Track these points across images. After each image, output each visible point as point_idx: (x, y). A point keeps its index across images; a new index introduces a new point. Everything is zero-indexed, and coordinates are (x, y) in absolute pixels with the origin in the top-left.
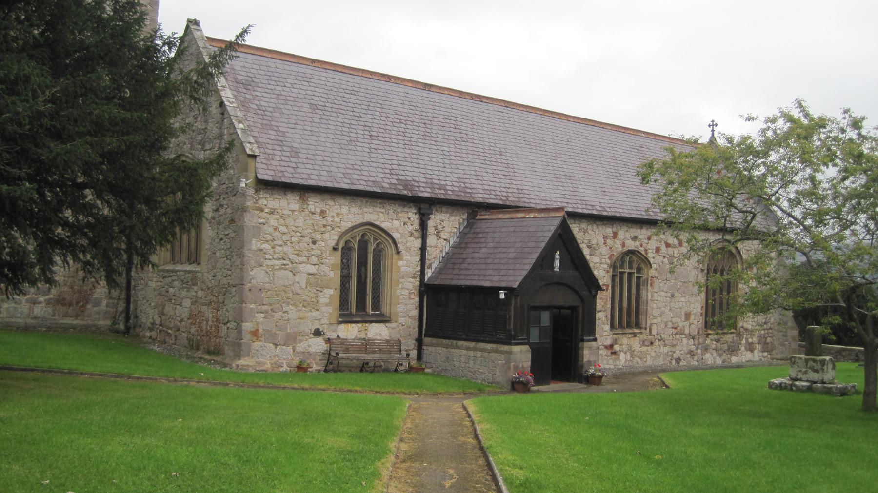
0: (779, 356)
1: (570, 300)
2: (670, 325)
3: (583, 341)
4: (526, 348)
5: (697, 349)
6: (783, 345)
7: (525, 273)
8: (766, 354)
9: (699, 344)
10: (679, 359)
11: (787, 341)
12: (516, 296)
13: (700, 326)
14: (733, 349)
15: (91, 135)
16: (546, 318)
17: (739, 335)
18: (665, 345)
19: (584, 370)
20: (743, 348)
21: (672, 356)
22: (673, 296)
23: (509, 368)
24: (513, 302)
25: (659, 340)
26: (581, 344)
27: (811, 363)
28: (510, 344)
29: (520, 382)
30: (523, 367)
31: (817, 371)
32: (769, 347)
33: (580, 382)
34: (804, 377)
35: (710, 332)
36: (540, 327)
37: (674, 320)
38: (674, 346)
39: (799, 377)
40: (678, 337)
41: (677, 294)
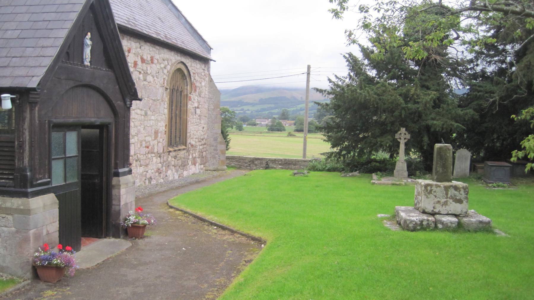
0: (211, 168)
1: (103, 116)
2: (144, 144)
3: (117, 175)
4: (51, 198)
5: (162, 167)
7: (48, 62)
8: (202, 166)
9: (164, 161)
10: (151, 178)
11: (217, 154)
12: (33, 104)
13: (165, 144)
14: (184, 166)
15: (240, 285)
16: (72, 142)
17: (188, 151)
18: (141, 166)
19: (122, 217)
20: (190, 163)
21: (146, 175)
22: (146, 114)
23: (26, 240)
24: (28, 115)
25: (136, 161)
26: (114, 180)
27: (452, 192)
28: (26, 195)
29: (51, 267)
30: (48, 233)
31: (460, 201)
33: (116, 236)
34: (443, 210)
35: (171, 149)
36: (65, 159)
37: (147, 138)
38: (147, 165)
39: (436, 210)
40: (149, 156)
41: (149, 113)
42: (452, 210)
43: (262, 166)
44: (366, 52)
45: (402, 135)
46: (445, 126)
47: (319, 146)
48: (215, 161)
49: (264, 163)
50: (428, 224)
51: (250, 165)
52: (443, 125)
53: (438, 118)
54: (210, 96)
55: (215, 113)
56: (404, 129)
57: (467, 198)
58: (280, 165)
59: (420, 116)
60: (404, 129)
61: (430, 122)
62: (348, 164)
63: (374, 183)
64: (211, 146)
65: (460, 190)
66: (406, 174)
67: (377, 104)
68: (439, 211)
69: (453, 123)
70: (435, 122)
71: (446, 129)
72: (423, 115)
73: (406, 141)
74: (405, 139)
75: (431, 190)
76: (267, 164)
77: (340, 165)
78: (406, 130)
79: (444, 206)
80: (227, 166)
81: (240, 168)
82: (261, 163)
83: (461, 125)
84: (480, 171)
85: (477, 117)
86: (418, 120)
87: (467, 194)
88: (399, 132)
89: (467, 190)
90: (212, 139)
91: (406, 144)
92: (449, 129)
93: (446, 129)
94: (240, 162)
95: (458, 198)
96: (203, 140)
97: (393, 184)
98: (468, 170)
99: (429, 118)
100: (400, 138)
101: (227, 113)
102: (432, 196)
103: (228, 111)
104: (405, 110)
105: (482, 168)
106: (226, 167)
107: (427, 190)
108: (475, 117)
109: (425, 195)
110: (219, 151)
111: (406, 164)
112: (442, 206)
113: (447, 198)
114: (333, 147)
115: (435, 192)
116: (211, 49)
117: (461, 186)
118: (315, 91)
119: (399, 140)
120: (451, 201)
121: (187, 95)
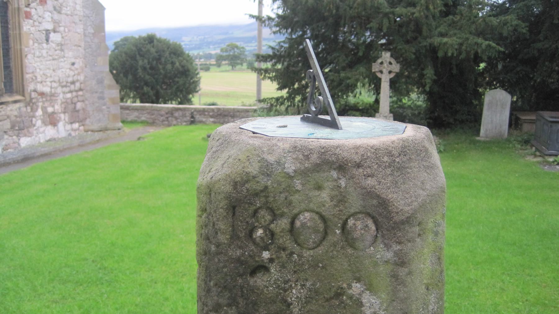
0: (95, 127)
6: (100, 110)
11: (105, 104)
20: (39, 123)
43: (185, 119)
45: (385, 65)
46: (464, 47)
47: (271, 89)
49: (187, 114)
51: (167, 118)
52: (461, 44)
53: (451, 33)
54: (87, 12)
56: (388, 54)
59: (418, 30)
60: (388, 54)
61: (437, 40)
67: (338, 8)
69: (480, 40)
70: (445, 40)
71: (468, 53)
72: (425, 28)
73: (392, 75)
74: (390, 72)
76: (192, 117)
78: (392, 56)
80: (123, 122)
81: (152, 123)
82: (184, 116)
83: (494, 45)
84: (526, 127)
85: (524, 31)
86: (415, 38)
88: (379, 61)
90: (94, 82)
91: (393, 83)
92: (472, 52)
93: (468, 53)
94: (153, 115)
96: (73, 83)
98: (506, 127)
99: (437, 33)
100: (381, 72)
101: (236, 50)
103: (237, 47)
104: (389, 18)
105: (532, 122)
106: (120, 124)
108: (520, 30)
114: (280, 89)
119: (379, 75)
121: (19, 9)
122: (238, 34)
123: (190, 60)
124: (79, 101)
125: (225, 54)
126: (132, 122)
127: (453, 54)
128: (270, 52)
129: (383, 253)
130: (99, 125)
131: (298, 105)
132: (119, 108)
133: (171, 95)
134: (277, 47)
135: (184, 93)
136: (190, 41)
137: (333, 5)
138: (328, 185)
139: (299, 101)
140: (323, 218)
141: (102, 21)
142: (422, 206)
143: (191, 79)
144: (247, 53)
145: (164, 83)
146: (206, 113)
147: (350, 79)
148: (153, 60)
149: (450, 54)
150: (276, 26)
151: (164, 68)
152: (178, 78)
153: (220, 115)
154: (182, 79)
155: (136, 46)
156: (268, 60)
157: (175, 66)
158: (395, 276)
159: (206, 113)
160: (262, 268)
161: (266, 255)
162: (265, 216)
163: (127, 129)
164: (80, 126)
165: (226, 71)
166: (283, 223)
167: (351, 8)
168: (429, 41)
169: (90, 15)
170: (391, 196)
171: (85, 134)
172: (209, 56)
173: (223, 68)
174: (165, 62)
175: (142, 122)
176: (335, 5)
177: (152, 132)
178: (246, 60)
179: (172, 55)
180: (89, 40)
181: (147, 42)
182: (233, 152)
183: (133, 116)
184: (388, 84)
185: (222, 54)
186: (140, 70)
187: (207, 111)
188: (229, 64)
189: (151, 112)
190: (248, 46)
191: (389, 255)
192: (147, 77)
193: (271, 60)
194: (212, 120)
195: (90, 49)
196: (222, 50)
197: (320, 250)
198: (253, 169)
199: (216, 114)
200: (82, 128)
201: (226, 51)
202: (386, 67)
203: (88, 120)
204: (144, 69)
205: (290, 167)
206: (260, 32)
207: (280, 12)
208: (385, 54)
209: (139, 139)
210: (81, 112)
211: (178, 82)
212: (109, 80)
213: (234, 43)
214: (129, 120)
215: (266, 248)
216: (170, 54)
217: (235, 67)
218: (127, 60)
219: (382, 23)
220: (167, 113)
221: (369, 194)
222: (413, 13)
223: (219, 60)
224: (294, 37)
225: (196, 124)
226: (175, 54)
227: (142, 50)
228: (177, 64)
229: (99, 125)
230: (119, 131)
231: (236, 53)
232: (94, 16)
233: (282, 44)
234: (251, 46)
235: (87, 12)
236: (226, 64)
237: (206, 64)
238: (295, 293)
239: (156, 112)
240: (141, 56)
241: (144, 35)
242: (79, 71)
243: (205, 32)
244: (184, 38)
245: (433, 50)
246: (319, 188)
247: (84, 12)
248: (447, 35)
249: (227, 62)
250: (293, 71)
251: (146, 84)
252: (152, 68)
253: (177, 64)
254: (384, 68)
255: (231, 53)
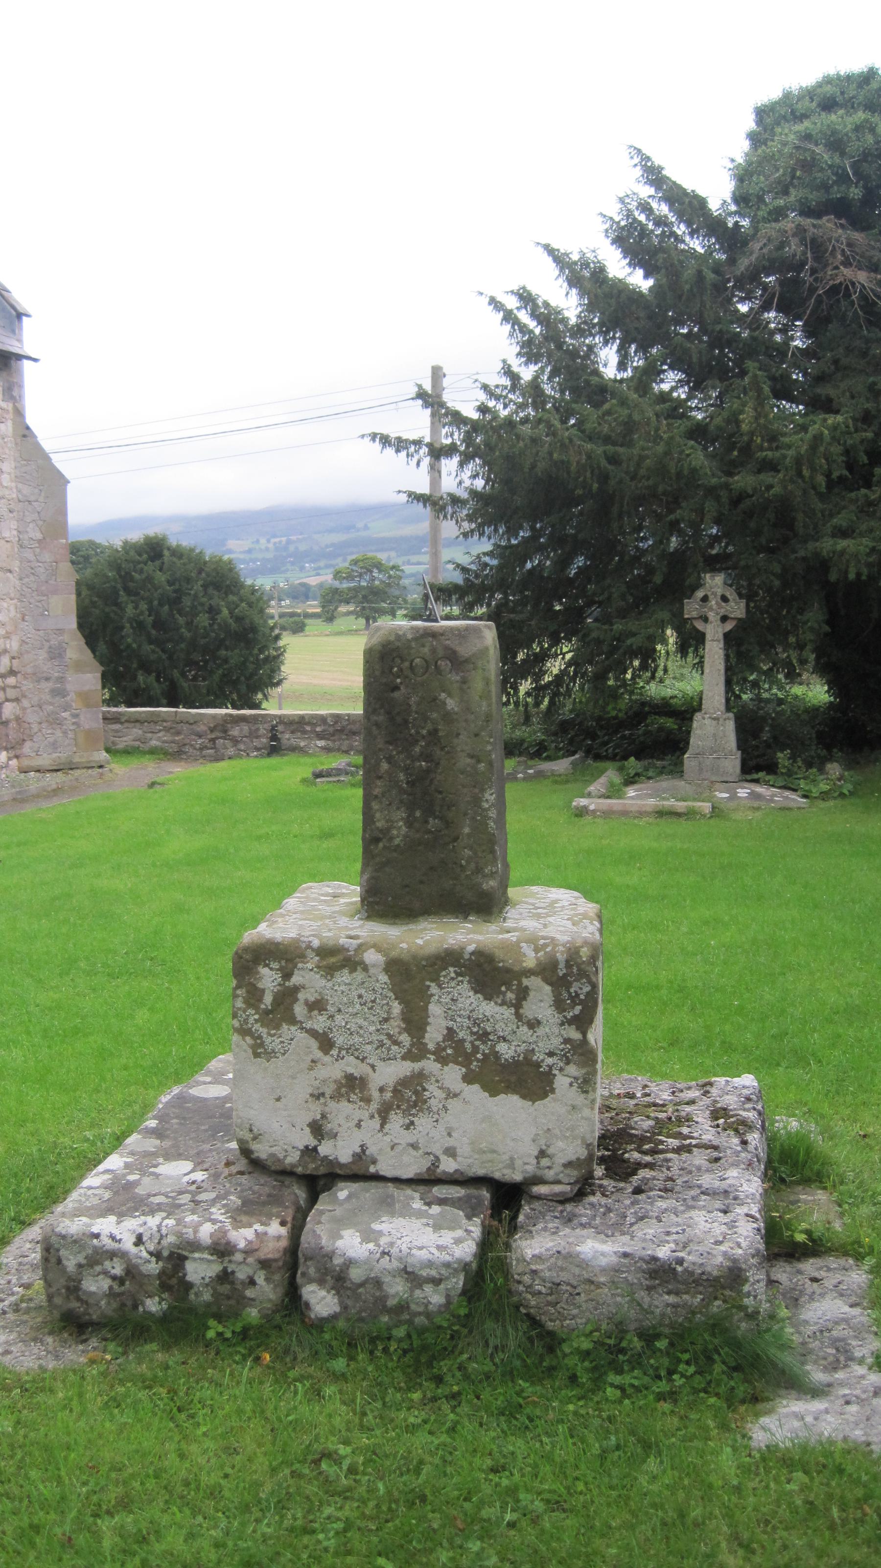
0: (45, 760)
6: (55, 721)
27: (454, 1005)
31: (526, 1079)
32: (13, 735)
34: (396, 1149)
39: (340, 1150)
42: (464, 1149)
43: (256, 743)
44: (585, 277)
48: (59, 733)
49: (262, 731)
50: (225, 1277)
51: (213, 740)
53: (864, 527)
55: (47, 557)
57: (582, 1053)
58: (320, 736)
61: (827, 545)
62: (564, 727)
63: (581, 812)
64: (39, 677)
65: (523, 994)
66: (733, 763)
68: (361, 1156)
70: (842, 544)
73: (729, 626)
74: (724, 619)
75: (287, 996)
76: (274, 738)
77: (534, 733)
79: (396, 1120)
80: (108, 750)
81: (177, 754)
82: (253, 735)
87: (583, 1022)
88: (700, 594)
89: (581, 988)
90: (43, 655)
94: (178, 733)
95: (506, 1051)
97: (661, 814)
100: (706, 620)
102: (294, 1040)
103: (379, 566)
104: (718, 499)
107: (254, 995)
109: (244, 1031)
110: (72, 696)
111: (730, 726)
112: (384, 1114)
113: (417, 1052)
115: (317, 1006)
116: (20, 316)
117: (530, 959)
118: (377, 445)
119: (699, 625)
120: (453, 1075)
122: (380, 529)
123: (256, 600)
124: (7, 700)
125: (345, 585)
126: (128, 752)
127: (859, 575)
128: (458, 578)
129: (455, 677)
130: (55, 755)
131: (526, 705)
132: (101, 716)
133: (208, 694)
134: (473, 567)
135: (243, 688)
136: (250, 551)
137: (592, 473)
138: (428, 644)
139: (528, 694)
140: (426, 661)
141: (62, 511)
142: (474, 655)
143: (261, 651)
144: (405, 582)
145: (191, 663)
146: (308, 728)
147: (634, 635)
148: (161, 605)
149: (852, 576)
150: (470, 518)
151: (189, 624)
152: (227, 649)
153: (341, 731)
154: (237, 651)
155: (119, 568)
156: (454, 598)
157: (219, 618)
158: (461, 689)
159: (308, 728)
160: (396, 688)
161: (399, 680)
162: (398, 661)
163: (119, 768)
164: (9, 759)
165: (350, 632)
166: (407, 664)
167: (632, 479)
168: (811, 546)
169: (32, 498)
170: (458, 649)
171: (22, 776)
172: (302, 593)
173: (341, 623)
174: (193, 607)
175: (152, 752)
176: (596, 472)
177: (178, 772)
178: (405, 601)
179: (211, 590)
180: (31, 556)
181: (145, 556)
182: (382, 632)
183: (130, 736)
184: (722, 645)
185: (337, 584)
186: (128, 630)
187: (309, 723)
188: (357, 614)
189: (174, 726)
190: (409, 563)
191: (458, 678)
192: (148, 648)
193: (461, 597)
194: (321, 743)
195: (32, 578)
196: (337, 575)
197: (425, 677)
198: (392, 638)
199: (331, 729)
200: (14, 763)
201: (350, 577)
202: (715, 607)
203: (28, 744)
204: (139, 626)
205: (410, 636)
206: (435, 530)
207: (479, 484)
208: (712, 578)
209: (152, 785)
210: (13, 725)
211: (226, 661)
212: (76, 649)
213: (370, 555)
214: (121, 746)
215: (399, 677)
216: (205, 587)
217: (375, 621)
218: (93, 604)
219: (703, 509)
220: (212, 730)
221: (447, 648)
222: (769, 487)
223: (330, 602)
224: (514, 542)
225: (284, 755)
226: (217, 586)
227: (132, 579)
228: (225, 612)
229: (55, 755)
230: (100, 770)
231: (377, 583)
232: (41, 499)
233: (487, 559)
234: (419, 563)
235: (26, 490)
236: (349, 613)
237: (292, 615)
238: (413, 700)
239: (185, 727)
240: (129, 592)
241: (136, 536)
242: (9, 628)
243: (288, 524)
244: (232, 544)
245: (823, 565)
246: (423, 646)
247: (19, 491)
248: (853, 531)
249: (351, 608)
250: (511, 620)
251: (145, 666)
252: (158, 624)
253: (225, 612)
254: (711, 609)
255: (364, 584)
